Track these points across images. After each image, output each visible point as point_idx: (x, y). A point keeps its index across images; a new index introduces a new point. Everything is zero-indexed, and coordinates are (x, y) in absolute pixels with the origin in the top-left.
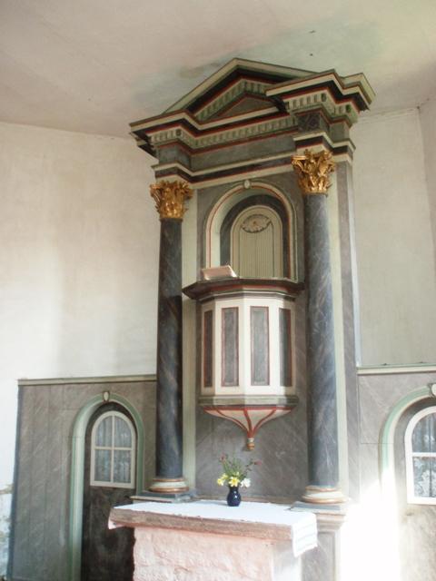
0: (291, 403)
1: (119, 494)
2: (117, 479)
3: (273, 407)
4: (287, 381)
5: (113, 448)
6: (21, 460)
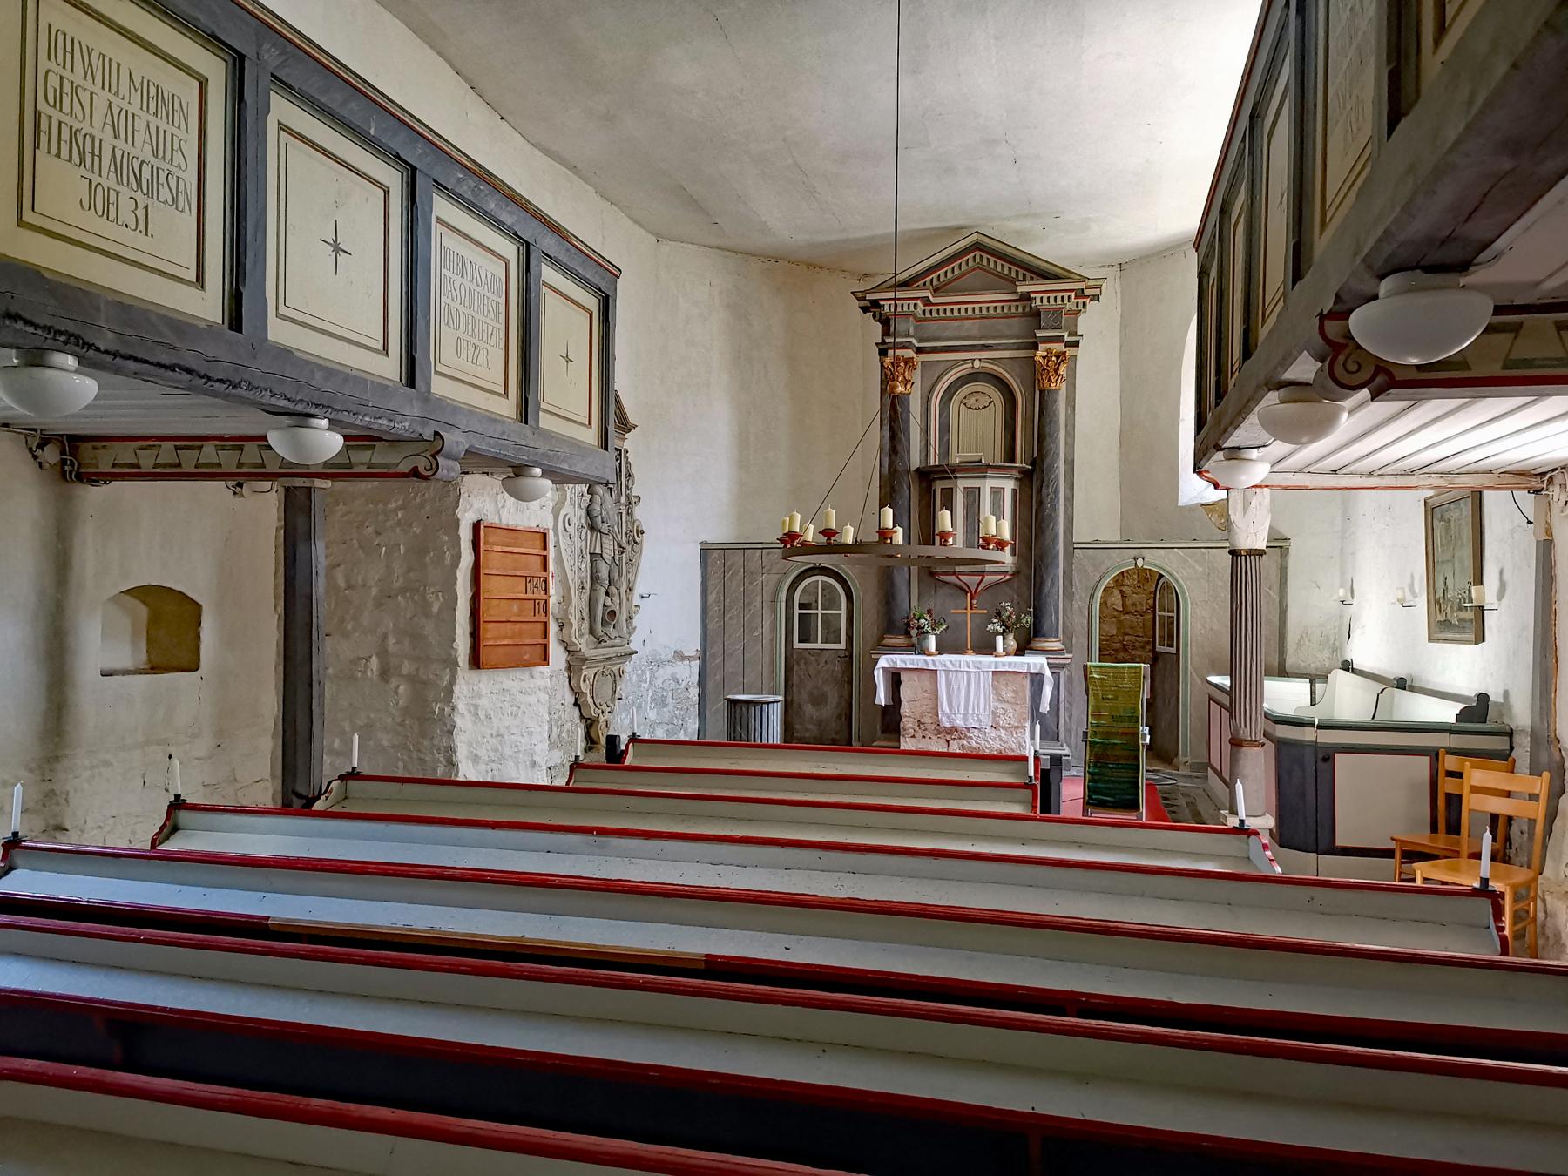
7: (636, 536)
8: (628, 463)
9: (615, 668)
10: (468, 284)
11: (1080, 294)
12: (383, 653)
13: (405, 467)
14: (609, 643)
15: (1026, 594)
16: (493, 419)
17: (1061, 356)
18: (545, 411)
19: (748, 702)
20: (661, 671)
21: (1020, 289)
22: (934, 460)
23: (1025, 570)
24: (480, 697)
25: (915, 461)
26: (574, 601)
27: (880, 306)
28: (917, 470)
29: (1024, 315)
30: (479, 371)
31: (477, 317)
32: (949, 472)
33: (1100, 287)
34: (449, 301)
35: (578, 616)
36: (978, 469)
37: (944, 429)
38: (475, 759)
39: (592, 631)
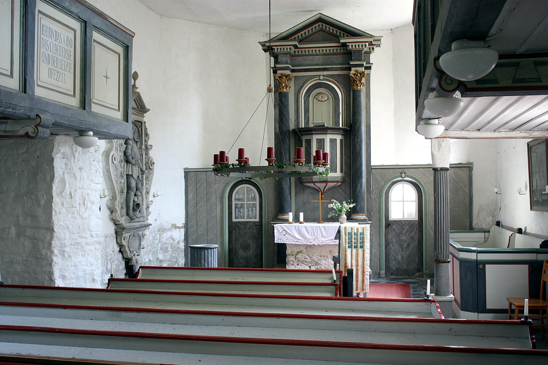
0: (343, 181)
1: (250, 224)
2: (248, 217)
3: (338, 182)
4: (342, 171)
5: (246, 203)
6: (190, 211)
7: (150, 165)
8: (146, 129)
9: (140, 233)
10: (54, 42)
11: (371, 44)
12: (17, 225)
13: (22, 132)
14: (136, 220)
15: (348, 192)
16: (66, 108)
17: (362, 74)
18: (94, 103)
19: (200, 248)
20: (165, 234)
21: (342, 41)
22: (303, 126)
23: (347, 179)
24: (65, 246)
25: (292, 126)
26: (118, 198)
27: (272, 49)
28: (293, 130)
29: (344, 54)
30: (59, 84)
31: (59, 58)
32: (309, 131)
33: (380, 40)
34: (45, 51)
35: (120, 206)
36: (322, 129)
37: (307, 110)
38: (63, 277)
39: (128, 214)
